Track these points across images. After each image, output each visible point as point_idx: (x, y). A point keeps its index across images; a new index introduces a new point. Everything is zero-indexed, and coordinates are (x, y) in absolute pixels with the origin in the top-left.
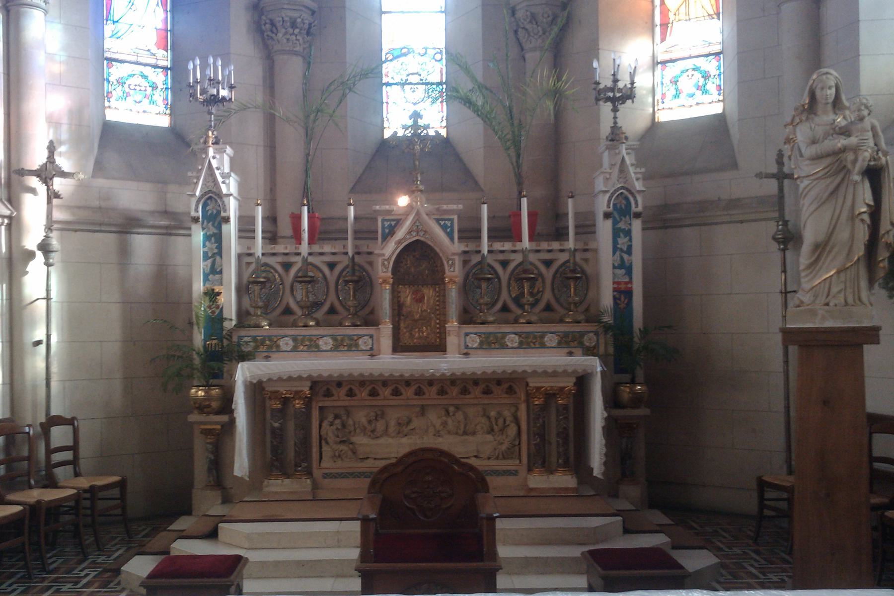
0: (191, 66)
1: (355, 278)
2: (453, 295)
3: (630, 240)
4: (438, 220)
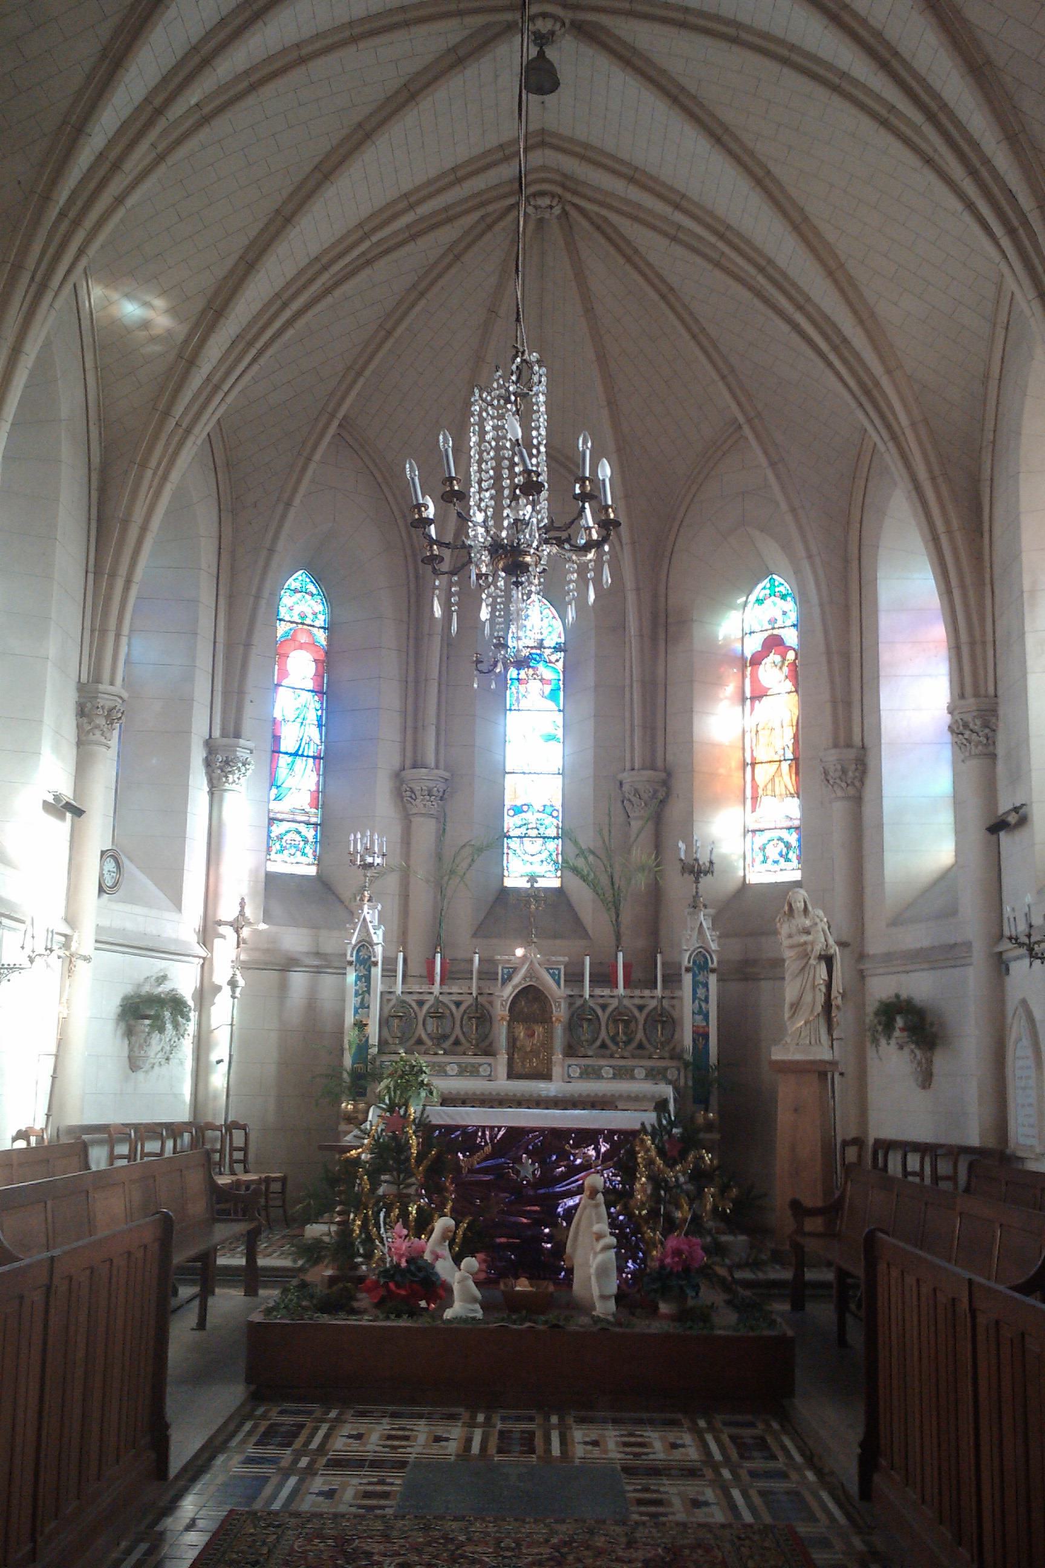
0: (352, 837)
1: (478, 1015)
2: (559, 1030)
3: (708, 990)
4: (547, 970)
